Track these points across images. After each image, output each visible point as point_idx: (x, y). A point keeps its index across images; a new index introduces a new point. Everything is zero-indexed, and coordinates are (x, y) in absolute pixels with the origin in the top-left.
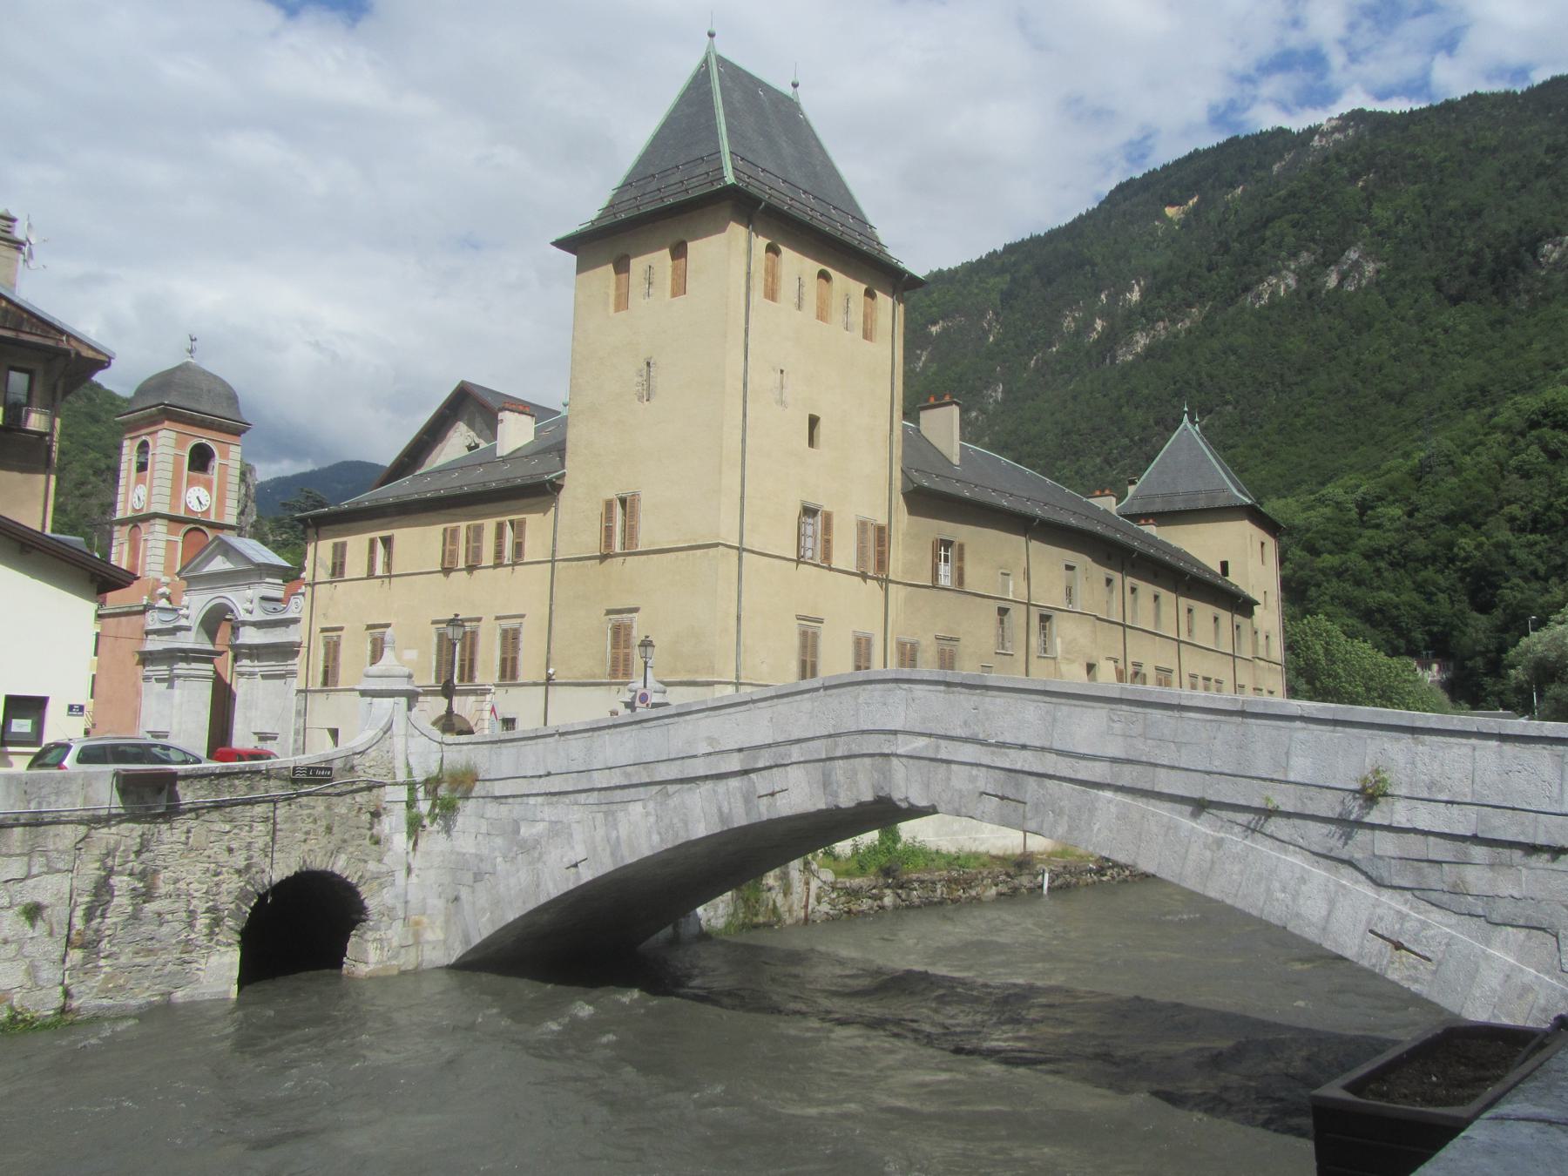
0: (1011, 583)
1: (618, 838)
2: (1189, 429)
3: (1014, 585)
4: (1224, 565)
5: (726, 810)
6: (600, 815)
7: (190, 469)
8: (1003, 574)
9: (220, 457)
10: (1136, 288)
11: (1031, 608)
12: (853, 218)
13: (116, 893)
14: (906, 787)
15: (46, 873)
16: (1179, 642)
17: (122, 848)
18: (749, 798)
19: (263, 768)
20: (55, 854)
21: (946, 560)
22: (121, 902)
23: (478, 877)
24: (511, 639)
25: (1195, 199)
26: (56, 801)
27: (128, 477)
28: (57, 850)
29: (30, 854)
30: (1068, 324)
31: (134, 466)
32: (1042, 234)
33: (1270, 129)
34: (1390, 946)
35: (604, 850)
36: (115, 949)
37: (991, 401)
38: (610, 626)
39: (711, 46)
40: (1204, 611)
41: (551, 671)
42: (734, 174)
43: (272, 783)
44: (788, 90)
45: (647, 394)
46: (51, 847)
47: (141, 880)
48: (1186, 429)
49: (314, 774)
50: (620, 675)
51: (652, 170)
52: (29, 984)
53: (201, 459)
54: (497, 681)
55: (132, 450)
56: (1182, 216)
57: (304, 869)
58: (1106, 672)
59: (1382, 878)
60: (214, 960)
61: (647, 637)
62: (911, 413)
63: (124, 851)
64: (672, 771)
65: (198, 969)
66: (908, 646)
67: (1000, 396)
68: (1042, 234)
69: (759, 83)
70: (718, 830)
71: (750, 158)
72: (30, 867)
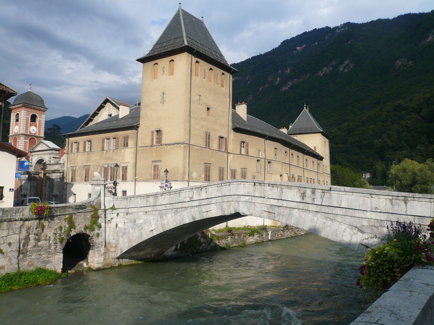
0: (260, 153)
1: (164, 223)
2: (306, 110)
3: (261, 154)
4: (315, 147)
5: (194, 216)
6: (159, 217)
7: (31, 121)
8: (258, 151)
9: (39, 118)
10: (289, 69)
11: (266, 160)
12: (219, 54)
13: (31, 239)
14: (242, 210)
15: (13, 234)
16: (304, 168)
17: (32, 228)
18: (201, 212)
19: (68, 205)
20: (15, 229)
21: (243, 147)
22: (32, 242)
23: (124, 234)
24: (125, 169)
25: (305, 45)
26: (15, 215)
27: (13, 124)
28: (15, 228)
29: (8, 229)
30: (270, 79)
31: (15, 120)
32: (263, 54)
33: (325, 27)
34: (365, 247)
35: (160, 227)
36: (31, 254)
37: (249, 100)
38: (153, 165)
39: (180, 6)
40: (311, 159)
41: (136, 178)
42: (187, 42)
43: (70, 209)
44: (201, 19)
45: (163, 102)
46: (14, 227)
47: (37, 236)
48: (305, 110)
49: (81, 207)
50: (156, 179)
51: (164, 40)
52: (9, 264)
53: (33, 118)
54: (121, 180)
55: (14, 116)
56: (301, 50)
57: (79, 233)
58: (285, 177)
59: (364, 231)
60: (56, 256)
61: (166, 169)
62: (234, 107)
63: (33, 228)
64: (180, 205)
65: (52, 259)
66: (233, 170)
67: (251, 98)
68: (263, 54)
69: (193, 17)
70: (192, 221)
71: (191, 38)
72: (9, 233)
